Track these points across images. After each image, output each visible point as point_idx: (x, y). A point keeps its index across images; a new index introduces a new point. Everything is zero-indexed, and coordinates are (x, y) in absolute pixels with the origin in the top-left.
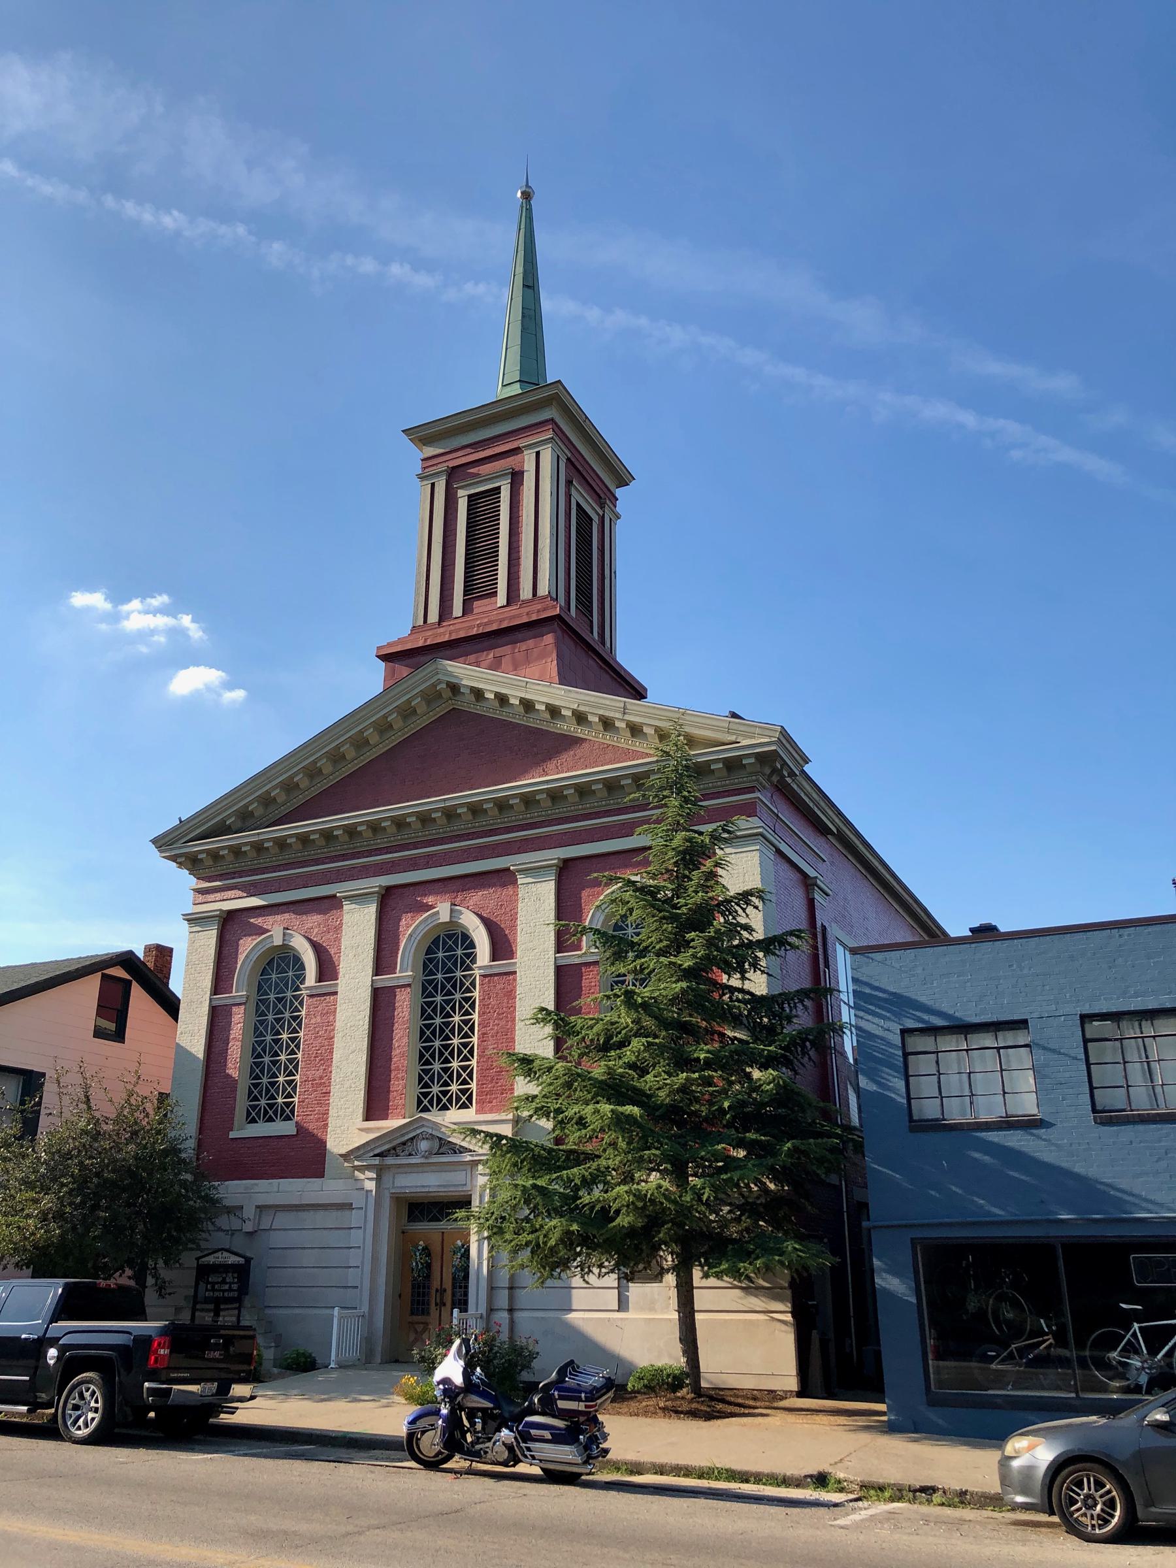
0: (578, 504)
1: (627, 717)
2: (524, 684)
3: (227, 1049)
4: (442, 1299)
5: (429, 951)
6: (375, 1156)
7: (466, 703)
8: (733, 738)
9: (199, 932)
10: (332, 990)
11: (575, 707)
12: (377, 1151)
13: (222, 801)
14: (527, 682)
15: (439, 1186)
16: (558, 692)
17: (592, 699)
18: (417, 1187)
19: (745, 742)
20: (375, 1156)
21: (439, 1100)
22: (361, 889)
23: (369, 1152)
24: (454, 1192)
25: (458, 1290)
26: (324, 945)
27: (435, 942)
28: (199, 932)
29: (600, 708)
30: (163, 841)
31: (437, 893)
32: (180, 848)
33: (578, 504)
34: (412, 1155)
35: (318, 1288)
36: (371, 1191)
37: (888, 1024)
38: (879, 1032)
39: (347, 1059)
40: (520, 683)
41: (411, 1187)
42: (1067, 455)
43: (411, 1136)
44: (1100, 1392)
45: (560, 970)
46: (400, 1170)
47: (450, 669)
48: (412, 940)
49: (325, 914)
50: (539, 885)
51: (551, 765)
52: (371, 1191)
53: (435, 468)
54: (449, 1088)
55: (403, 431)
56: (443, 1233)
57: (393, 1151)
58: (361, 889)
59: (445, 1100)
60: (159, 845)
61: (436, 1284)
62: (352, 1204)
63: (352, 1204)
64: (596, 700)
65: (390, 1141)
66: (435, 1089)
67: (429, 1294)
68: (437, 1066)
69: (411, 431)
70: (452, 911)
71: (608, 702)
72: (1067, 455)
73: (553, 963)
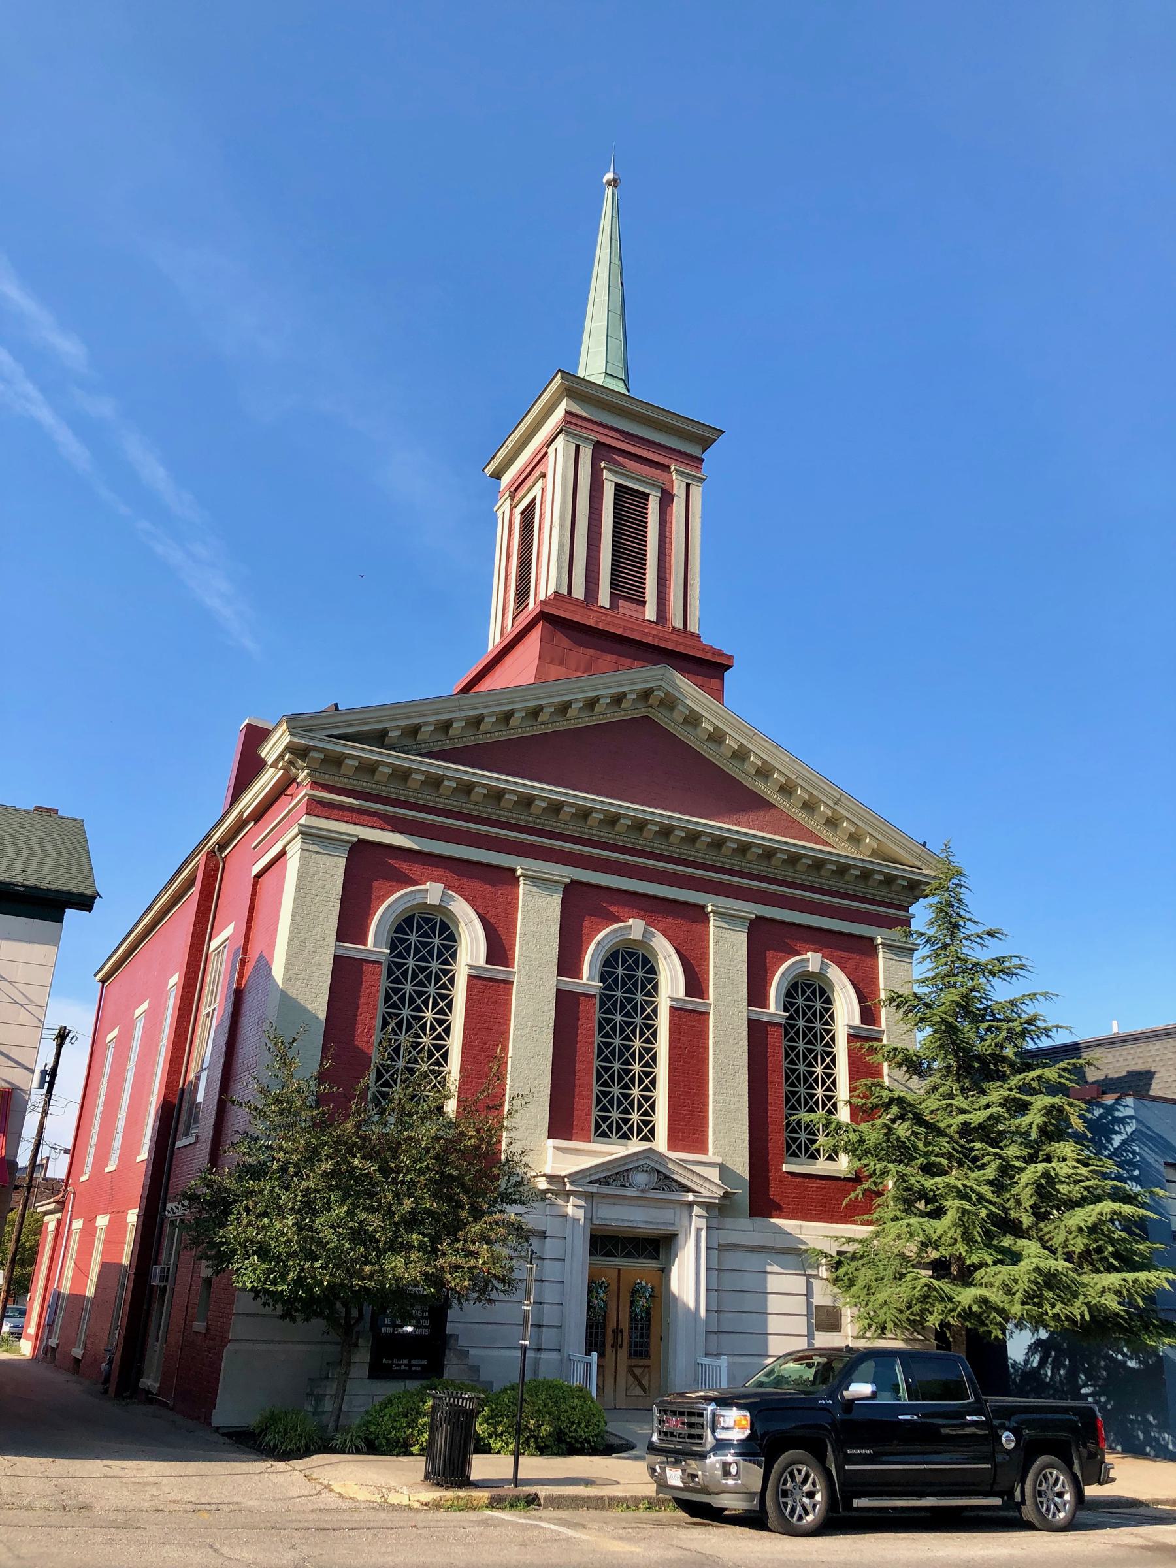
0: (534, 499)
1: (836, 807)
2: (752, 734)
3: (357, 1015)
4: (616, 1338)
5: (399, 929)
6: (591, 1182)
7: (671, 723)
8: (918, 864)
9: (317, 853)
10: (504, 977)
11: (794, 777)
12: (594, 1178)
13: (405, 706)
14: (756, 734)
15: (646, 1222)
16: (783, 757)
17: (813, 778)
18: (622, 1220)
19: (926, 871)
20: (591, 1182)
21: (619, 1128)
22: (545, 873)
23: (585, 1177)
24: (662, 1230)
25: (633, 1331)
26: (491, 920)
27: (409, 920)
28: (317, 853)
29: (816, 789)
30: (301, 724)
31: (625, 905)
32: (319, 739)
33: (534, 499)
34: (624, 1186)
35: (494, 1326)
36: (579, 1220)
37: (1157, 1157)
38: (1152, 1161)
39: (528, 1063)
40: (747, 731)
41: (617, 1220)
42: (45, 415)
43: (635, 1165)
44: (751, 1403)
45: (752, 1023)
46: (604, 1200)
47: (678, 682)
48: (601, 947)
49: (493, 885)
50: (732, 933)
51: (744, 817)
52: (579, 1220)
53: (579, 429)
54: (630, 1116)
55: (723, 432)
56: (619, 1270)
57: (606, 1181)
58: (545, 873)
59: (625, 1128)
60: (293, 724)
61: (612, 1324)
62: (545, 1232)
63: (545, 1232)
64: (817, 781)
65: (610, 1169)
66: (615, 1115)
67: (604, 1335)
68: (616, 1090)
69: (569, 377)
70: (645, 931)
71: (826, 788)
72: (45, 415)
73: (746, 1014)
